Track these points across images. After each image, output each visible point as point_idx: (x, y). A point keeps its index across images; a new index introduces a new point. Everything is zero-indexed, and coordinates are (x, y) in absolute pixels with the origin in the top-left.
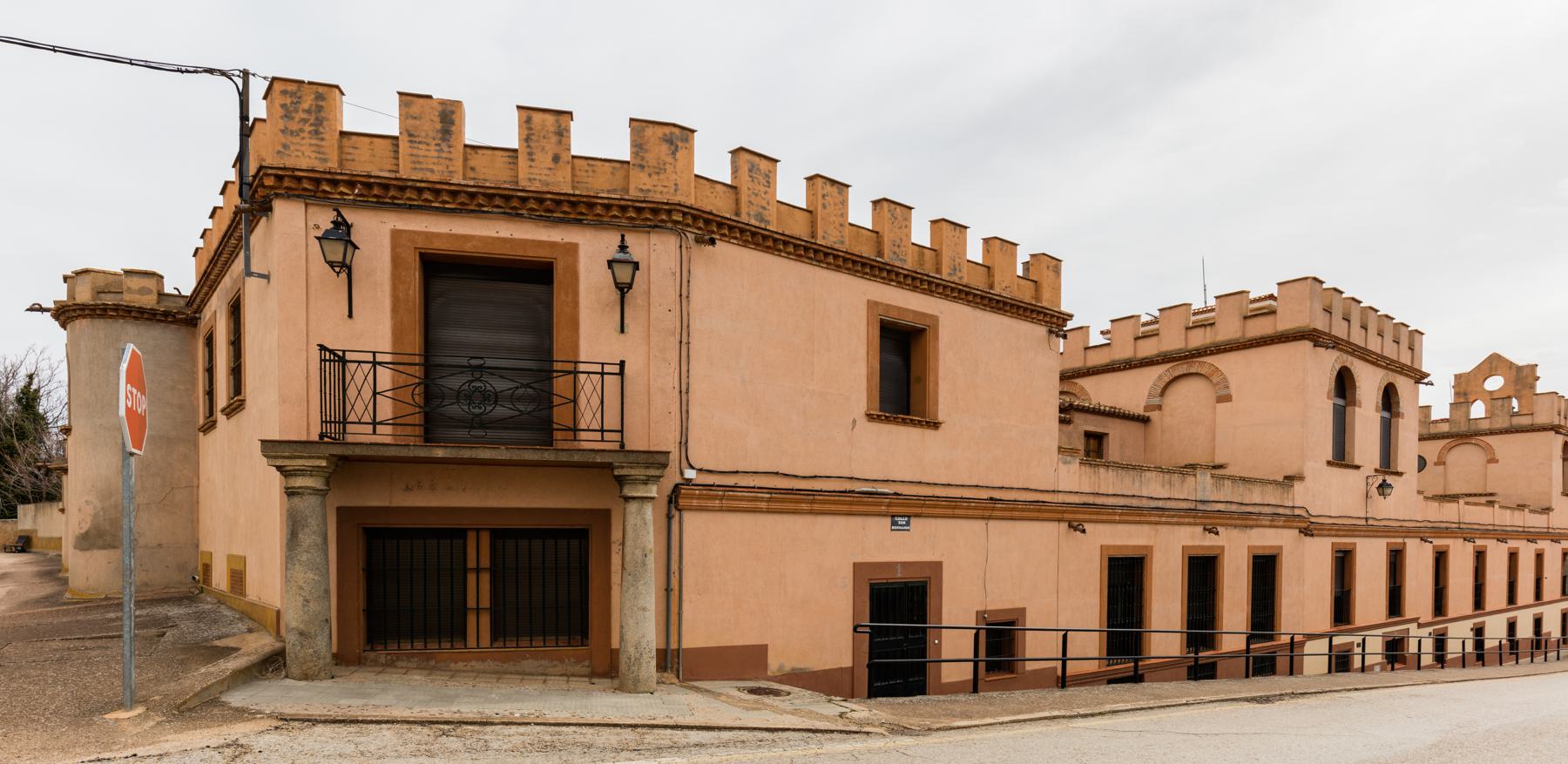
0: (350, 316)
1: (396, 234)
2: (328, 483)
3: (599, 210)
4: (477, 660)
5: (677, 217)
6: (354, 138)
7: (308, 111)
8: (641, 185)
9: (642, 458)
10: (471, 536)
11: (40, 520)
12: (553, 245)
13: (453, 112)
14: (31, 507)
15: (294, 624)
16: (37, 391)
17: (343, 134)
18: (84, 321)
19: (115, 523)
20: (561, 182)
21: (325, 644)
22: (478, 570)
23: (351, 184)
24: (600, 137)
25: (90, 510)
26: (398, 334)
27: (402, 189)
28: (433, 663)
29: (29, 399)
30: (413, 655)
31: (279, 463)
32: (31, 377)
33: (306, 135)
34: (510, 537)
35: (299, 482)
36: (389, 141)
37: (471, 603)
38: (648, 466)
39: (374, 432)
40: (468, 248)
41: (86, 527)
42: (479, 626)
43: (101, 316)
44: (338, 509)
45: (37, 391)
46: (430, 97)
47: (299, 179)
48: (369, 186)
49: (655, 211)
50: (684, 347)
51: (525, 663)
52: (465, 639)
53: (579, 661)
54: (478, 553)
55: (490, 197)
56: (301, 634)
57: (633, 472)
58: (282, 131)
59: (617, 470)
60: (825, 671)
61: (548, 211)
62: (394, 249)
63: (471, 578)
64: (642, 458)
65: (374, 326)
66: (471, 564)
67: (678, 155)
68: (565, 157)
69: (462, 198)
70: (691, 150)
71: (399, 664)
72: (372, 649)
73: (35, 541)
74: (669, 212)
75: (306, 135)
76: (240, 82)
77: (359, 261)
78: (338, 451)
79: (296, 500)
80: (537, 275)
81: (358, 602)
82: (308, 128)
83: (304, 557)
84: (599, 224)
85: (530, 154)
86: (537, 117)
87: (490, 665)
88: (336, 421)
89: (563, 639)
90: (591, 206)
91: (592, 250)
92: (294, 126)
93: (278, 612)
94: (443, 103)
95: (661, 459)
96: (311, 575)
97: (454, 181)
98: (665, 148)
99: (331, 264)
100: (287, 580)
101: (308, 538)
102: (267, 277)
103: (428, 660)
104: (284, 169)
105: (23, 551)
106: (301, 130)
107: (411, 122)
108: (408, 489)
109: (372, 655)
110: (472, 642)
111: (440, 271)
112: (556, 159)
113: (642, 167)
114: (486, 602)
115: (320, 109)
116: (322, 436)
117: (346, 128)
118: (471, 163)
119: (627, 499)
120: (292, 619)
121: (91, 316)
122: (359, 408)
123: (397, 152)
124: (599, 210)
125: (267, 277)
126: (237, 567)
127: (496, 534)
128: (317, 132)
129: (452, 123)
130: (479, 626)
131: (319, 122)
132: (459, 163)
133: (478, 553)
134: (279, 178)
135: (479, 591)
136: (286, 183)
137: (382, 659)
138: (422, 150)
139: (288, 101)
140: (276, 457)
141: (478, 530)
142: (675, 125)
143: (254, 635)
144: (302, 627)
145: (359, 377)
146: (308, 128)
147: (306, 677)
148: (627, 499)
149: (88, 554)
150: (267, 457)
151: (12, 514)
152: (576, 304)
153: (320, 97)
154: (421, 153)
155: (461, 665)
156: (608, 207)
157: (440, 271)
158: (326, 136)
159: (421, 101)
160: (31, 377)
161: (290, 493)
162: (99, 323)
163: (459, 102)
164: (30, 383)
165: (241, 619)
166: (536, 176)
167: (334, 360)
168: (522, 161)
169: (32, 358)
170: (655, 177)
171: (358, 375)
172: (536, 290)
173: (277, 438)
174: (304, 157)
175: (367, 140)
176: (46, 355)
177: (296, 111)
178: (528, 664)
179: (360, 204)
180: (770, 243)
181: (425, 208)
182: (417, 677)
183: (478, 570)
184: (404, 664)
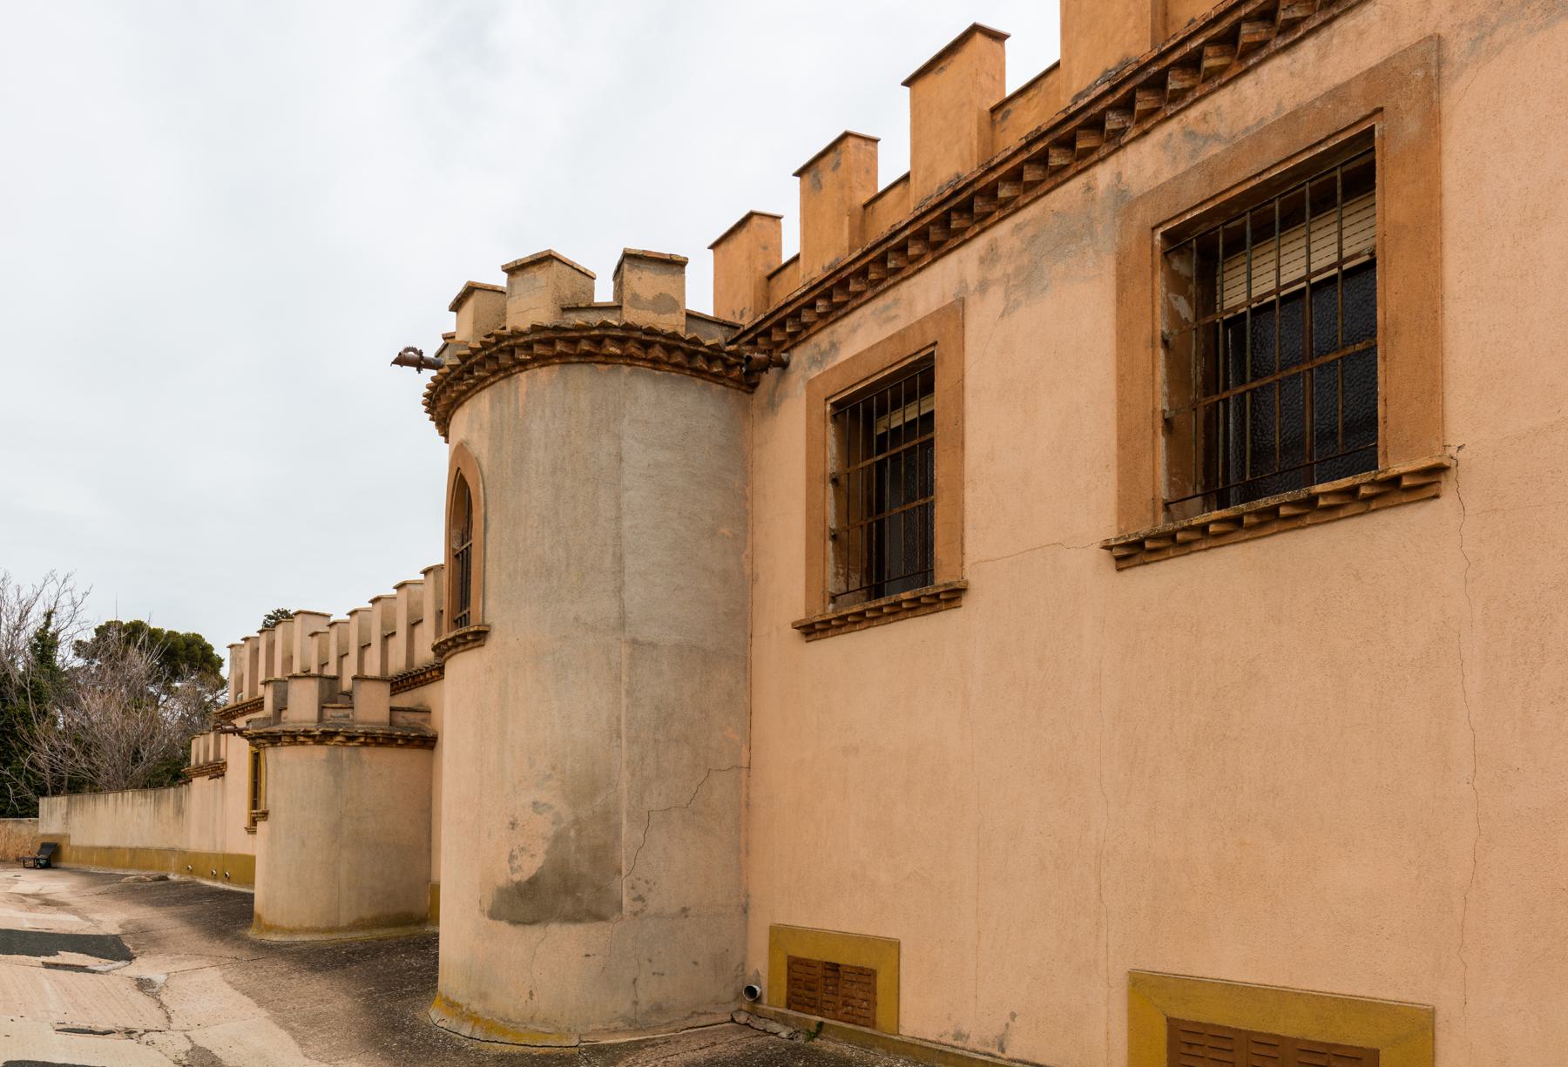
11: (76, 820)
14: (61, 801)
16: (55, 636)
18: (543, 375)
19: (602, 856)
25: (543, 826)
29: (45, 645)
32: (49, 615)
41: (529, 867)
43: (587, 358)
45: (55, 636)
60: (1130, 1030)
73: (66, 852)
105: (47, 866)
121: (564, 359)
130: (429, 929)
149: (535, 932)
151: (30, 811)
160: (49, 615)
162: (582, 377)
164: (48, 624)
169: (52, 589)
176: (69, 584)
180: (585, 346)
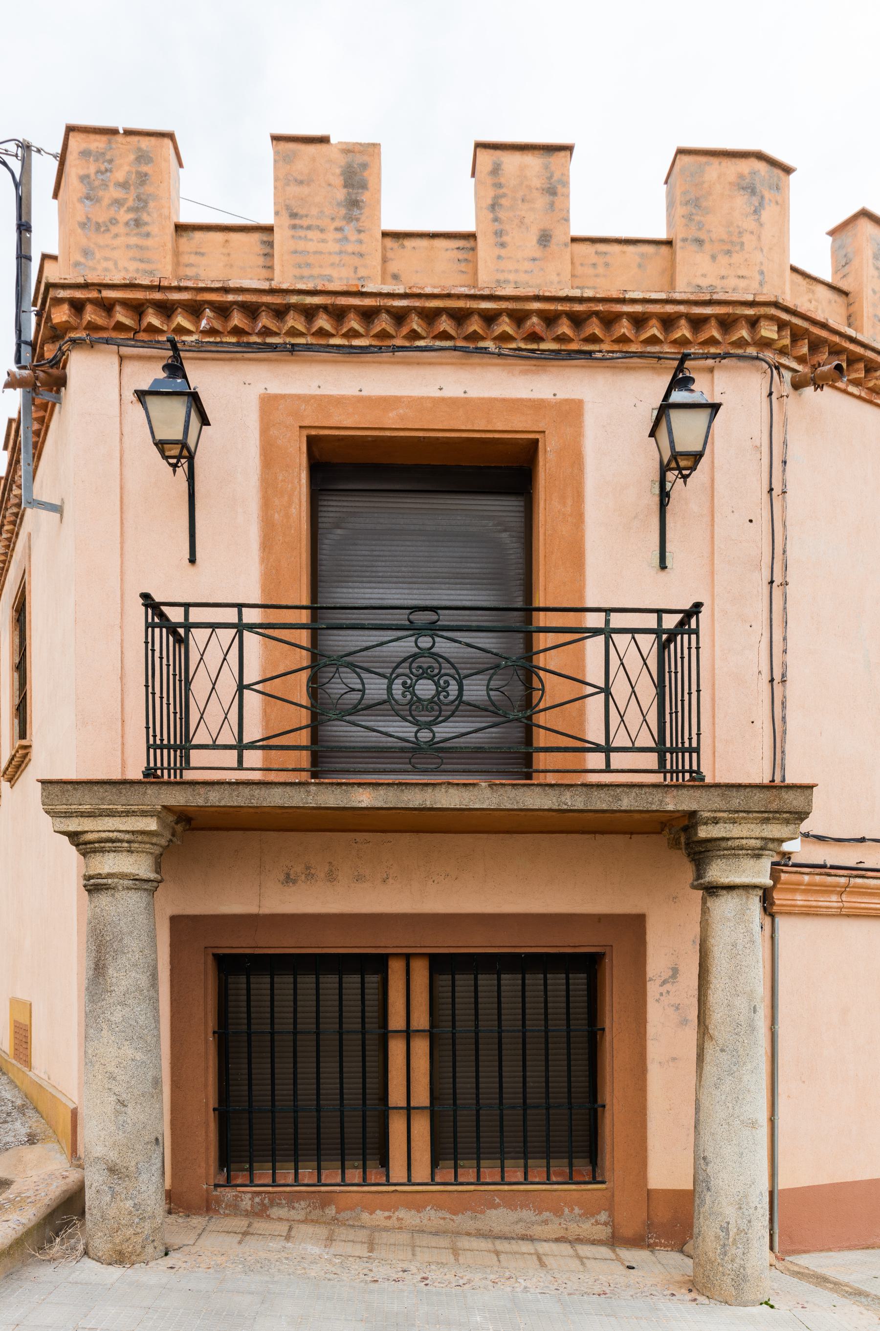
0: (192, 560)
1: (268, 402)
2: (158, 869)
3: (625, 328)
4: (409, 1206)
5: (768, 331)
6: (198, 235)
7: (124, 185)
8: (699, 275)
9: (758, 800)
10: (396, 969)
12: (538, 406)
13: (365, 166)
15: (98, 1150)
17: (181, 229)
20: (555, 278)
21: (150, 1187)
22: (408, 1034)
23: (195, 310)
24: (618, 197)
26: (271, 576)
27: (280, 313)
28: (331, 1211)
30: (299, 1196)
31: (73, 825)
33: (120, 229)
34: (469, 969)
35: (108, 864)
36: (256, 237)
37: (396, 1097)
38: (768, 816)
39: (240, 767)
40: (392, 422)
42: (410, 1139)
44: (175, 920)
46: (324, 140)
47: (107, 307)
48: (223, 311)
49: (726, 324)
50: (777, 593)
51: (492, 1213)
52: (385, 1162)
53: (589, 1213)
54: (409, 1000)
55: (430, 316)
56: (112, 1170)
57: (735, 831)
58: (83, 225)
59: (678, 834)
60: (818, 1186)
61: (534, 337)
62: (265, 430)
63: (396, 1048)
64: (758, 800)
65: (242, 551)
66: (396, 1021)
67: (765, 215)
68: (559, 237)
69: (384, 323)
70: (783, 206)
71: (275, 1212)
72: (229, 1183)
74: (753, 323)
75: (120, 229)
76: (16, 165)
77: (209, 447)
78: (177, 798)
79: (104, 899)
80: (501, 472)
81: (206, 1095)
82: (124, 216)
83: (117, 1015)
84: (625, 357)
85: (499, 233)
86: (511, 161)
87: (431, 1217)
88: (173, 744)
89: (560, 1166)
90: (609, 321)
91: (605, 415)
92: (102, 217)
93: (74, 1113)
94: (348, 150)
95: (794, 800)
96: (128, 1051)
97: (370, 288)
98: (741, 202)
99: (161, 445)
100: (88, 1061)
101: (125, 976)
102: (58, 509)
103: (324, 1205)
104: (86, 286)
106: (113, 221)
107: (294, 190)
108: (289, 880)
109: (229, 1194)
110: (398, 1171)
111: (345, 469)
112: (545, 239)
113: (700, 242)
114: (422, 1096)
115: (143, 178)
116: (149, 772)
117: (186, 217)
118: (393, 267)
119: (712, 890)
120: (96, 1138)
122: (211, 720)
123: (269, 255)
124: (625, 328)
125: (58, 509)
126: (23, 1020)
127: (440, 964)
128: (138, 223)
129: (364, 186)
130: (410, 1139)
131: (142, 203)
132: (375, 261)
133: (409, 1000)
134: (78, 306)
135: (410, 1072)
136: (90, 315)
137: (246, 1203)
138: (312, 242)
139: (92, 170)
140: (68, 815)
141: (408, 957)
142: (760, 156)
143: (38, 1148)
144: (113, 1156)
145: (213, 657)
146: (124, 216)
147: (120, 1258)
148: (712, 890)
150: (53, 814)
152: (579, 517)
153: (143, 157)
154: (311, 247)
155: (380, 1214)
156: (639, 321)
157: (345, 469)
158: (154, 229)
159: (312, 149)
161: (95, 886)
163: (376, 146)
165: (22, 1110)
166: (514, 271)
167: (167, 625)
168: (484, 245)
170: (723, 260)
171: (209, 650)
172: (501, 508)
173: (73, 776)
174: (117, 264)
175: (219, 236)
177: (105, 185)
178: (499, 1218)
179: (213, 349)
181: (319, 348)
182: (309, 1245)
183: (408, 1034)
184: (282, 1212)
